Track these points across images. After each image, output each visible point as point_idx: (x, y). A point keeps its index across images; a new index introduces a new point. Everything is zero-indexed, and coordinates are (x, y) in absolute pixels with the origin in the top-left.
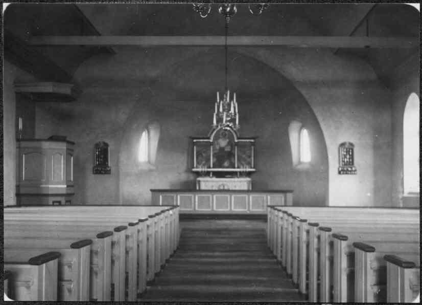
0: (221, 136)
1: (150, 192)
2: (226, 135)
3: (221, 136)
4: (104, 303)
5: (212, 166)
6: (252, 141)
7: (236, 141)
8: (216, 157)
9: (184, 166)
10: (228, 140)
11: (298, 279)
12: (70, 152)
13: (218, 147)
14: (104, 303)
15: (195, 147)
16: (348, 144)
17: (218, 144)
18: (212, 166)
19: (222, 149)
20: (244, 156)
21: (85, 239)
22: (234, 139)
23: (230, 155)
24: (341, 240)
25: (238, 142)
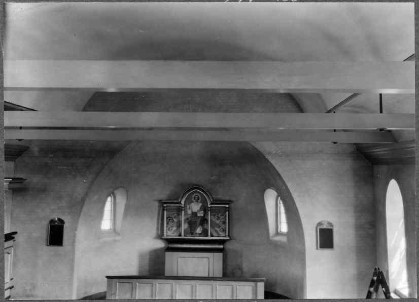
0: (193, 200)
1: (106, 279)
2: (198, 199)
3: (193, 200)
4: (237, 301)
5: (183, 234)
6: (227, 206)
7: (209, 206)
8: (189, 223)
9: (154, 231)
10: (201, 204)
11: (399, 296)
12: (17, 186)
13: (189, 212)
14: (237, 301)
15: (165, 212)
16: (326, 224)
17: (189, 208)
18: (183, 234)
19: (194, 214)
20: (218, 222)
21: (168, 62)
22: (208, 205)
23: (204, 221)
24: (209, 277)
25: (211, 207)
